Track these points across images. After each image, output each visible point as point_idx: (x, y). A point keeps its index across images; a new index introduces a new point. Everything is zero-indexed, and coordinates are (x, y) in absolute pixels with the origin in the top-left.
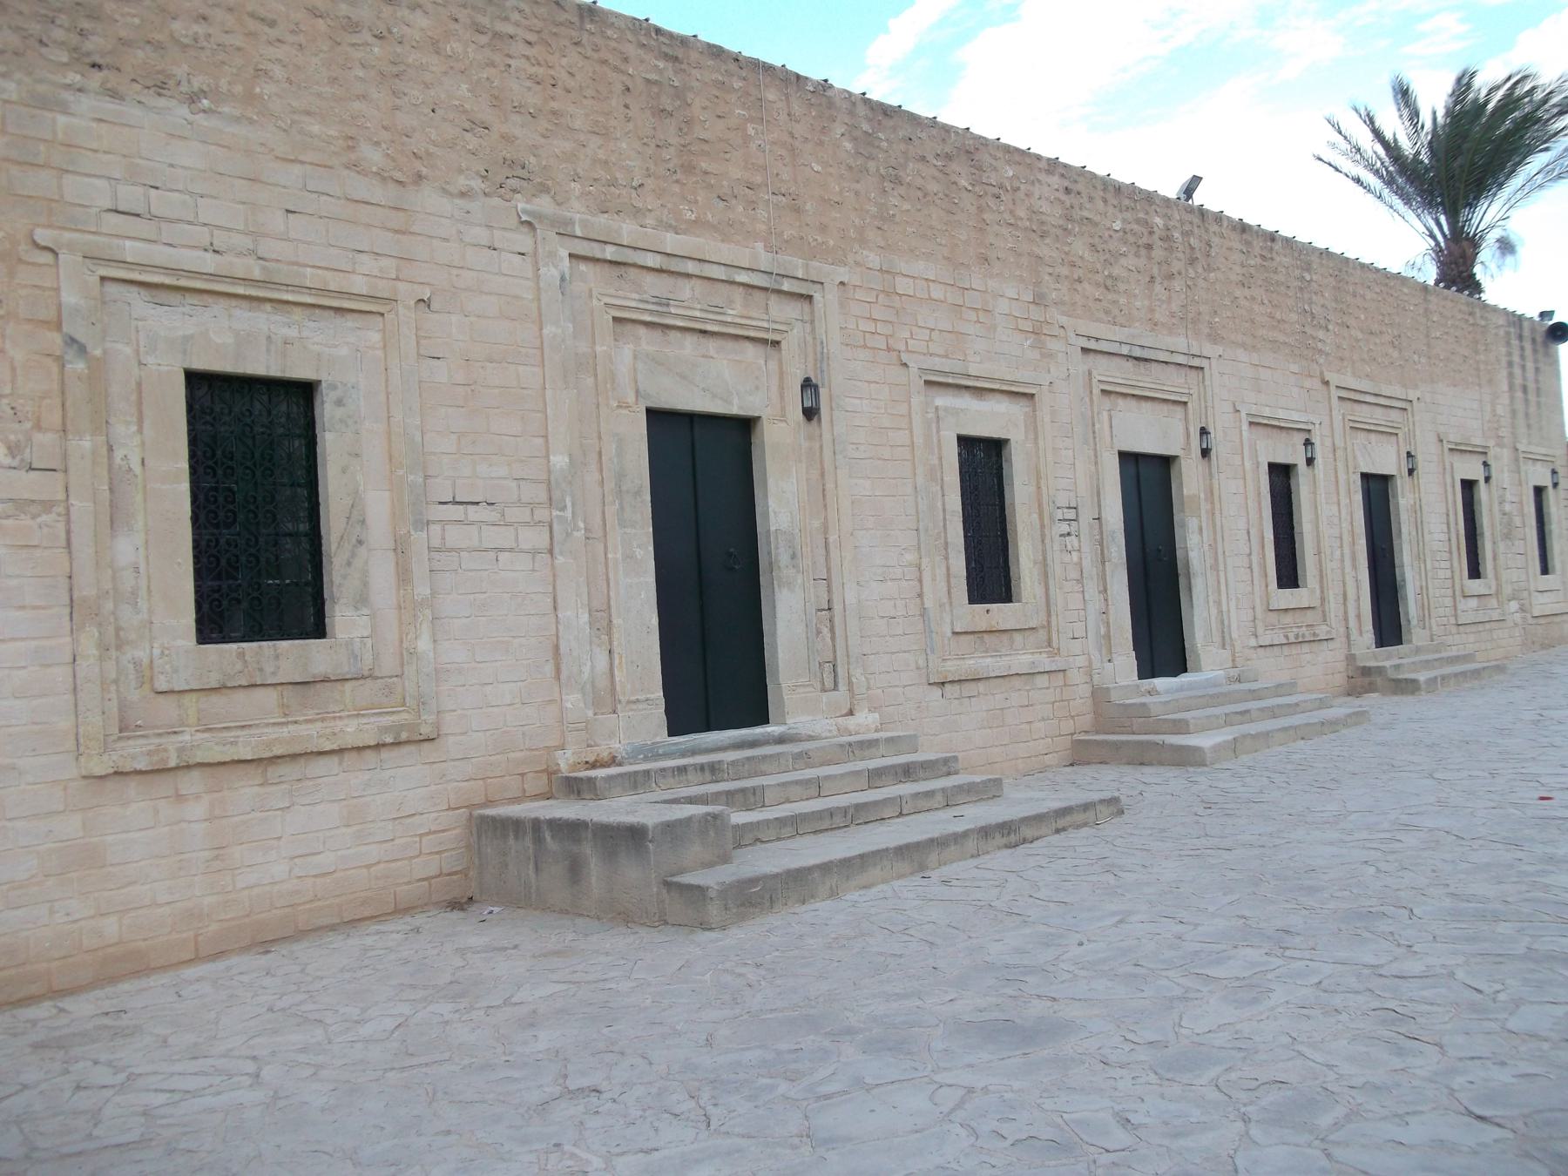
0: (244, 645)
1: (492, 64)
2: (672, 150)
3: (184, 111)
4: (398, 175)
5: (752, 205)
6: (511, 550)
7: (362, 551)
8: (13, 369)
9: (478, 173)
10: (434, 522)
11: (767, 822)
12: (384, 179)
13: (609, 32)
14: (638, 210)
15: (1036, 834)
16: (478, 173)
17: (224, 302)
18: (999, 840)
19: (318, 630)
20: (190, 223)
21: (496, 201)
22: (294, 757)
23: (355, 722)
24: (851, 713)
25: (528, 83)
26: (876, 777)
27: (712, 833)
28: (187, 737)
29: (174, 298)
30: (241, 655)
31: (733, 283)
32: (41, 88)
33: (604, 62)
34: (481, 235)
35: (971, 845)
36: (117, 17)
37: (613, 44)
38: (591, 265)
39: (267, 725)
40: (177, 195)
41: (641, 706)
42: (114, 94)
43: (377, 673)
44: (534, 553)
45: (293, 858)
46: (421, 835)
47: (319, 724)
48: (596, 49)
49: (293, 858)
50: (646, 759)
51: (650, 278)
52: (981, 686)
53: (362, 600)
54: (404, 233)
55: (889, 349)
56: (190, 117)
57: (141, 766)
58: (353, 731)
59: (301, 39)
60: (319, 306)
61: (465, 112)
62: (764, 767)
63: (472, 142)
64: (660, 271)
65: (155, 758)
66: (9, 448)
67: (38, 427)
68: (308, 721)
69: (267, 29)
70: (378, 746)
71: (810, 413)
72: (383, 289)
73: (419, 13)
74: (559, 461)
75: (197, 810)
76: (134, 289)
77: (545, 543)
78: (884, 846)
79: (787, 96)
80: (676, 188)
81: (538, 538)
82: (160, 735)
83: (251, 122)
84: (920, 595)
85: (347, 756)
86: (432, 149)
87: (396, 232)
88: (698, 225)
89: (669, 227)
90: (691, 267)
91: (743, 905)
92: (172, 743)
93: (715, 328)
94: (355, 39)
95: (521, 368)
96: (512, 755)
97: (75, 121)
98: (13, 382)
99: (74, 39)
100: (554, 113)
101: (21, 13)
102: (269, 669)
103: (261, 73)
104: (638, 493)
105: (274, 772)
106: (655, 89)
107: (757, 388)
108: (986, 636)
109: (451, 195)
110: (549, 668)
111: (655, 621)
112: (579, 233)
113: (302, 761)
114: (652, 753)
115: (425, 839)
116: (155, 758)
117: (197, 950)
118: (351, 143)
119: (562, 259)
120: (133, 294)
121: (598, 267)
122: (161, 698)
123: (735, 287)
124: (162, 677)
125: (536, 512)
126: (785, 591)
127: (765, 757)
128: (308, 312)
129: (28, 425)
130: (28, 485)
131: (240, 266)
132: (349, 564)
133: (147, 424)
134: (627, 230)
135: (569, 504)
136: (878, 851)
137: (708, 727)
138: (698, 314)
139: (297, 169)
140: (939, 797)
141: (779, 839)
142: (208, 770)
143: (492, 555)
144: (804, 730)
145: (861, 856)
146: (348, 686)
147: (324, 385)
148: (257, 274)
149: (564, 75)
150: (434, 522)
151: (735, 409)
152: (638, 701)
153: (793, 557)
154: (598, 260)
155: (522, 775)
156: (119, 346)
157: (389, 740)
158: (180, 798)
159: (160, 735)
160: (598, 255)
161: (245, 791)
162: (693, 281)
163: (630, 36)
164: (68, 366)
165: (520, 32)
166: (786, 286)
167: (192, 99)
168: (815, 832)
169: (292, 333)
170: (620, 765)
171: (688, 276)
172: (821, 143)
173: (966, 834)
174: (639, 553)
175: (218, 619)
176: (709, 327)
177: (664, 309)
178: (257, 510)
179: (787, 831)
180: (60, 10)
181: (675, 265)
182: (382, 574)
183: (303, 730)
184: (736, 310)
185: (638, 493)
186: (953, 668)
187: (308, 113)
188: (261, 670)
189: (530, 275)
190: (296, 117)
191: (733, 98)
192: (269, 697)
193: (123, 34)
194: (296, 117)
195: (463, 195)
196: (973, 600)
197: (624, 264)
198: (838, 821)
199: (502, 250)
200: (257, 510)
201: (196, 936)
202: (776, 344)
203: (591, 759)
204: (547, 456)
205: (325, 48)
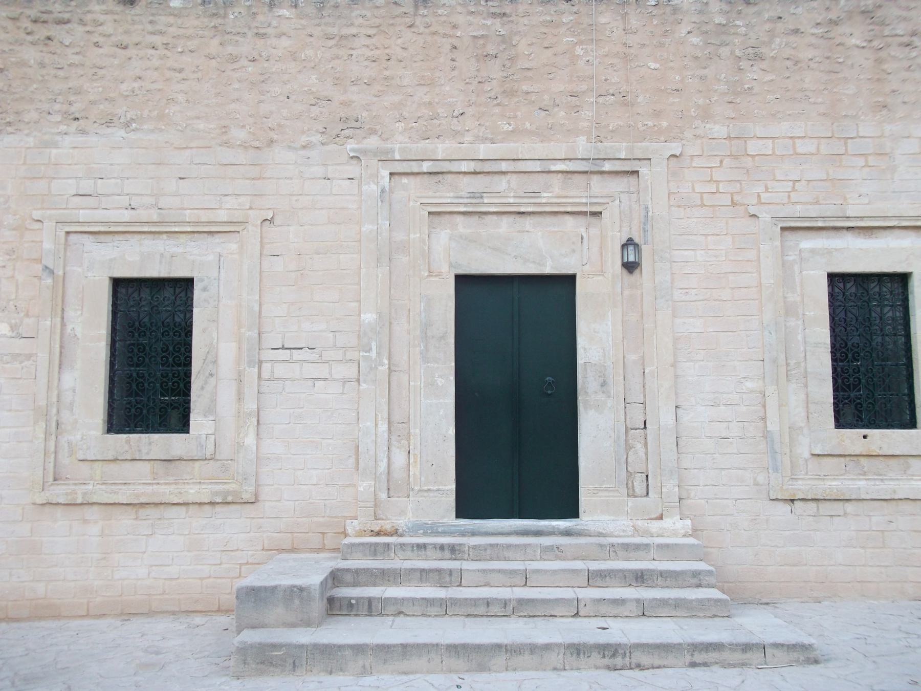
0: (131, 435)
1: (338, 57)
2: (494, 83)
3: (122, 133)
4: (257, 144)
5: (577, 109)
6: (326, 379)
7: (212, 380)
8: (17, 286)
9: (317, 131)
10: (266, 362)
11: (413, 601)
12: (245, 147)
13: (440, 12)
14: (457, 133)
15: (657, 662)
16: (317, 131)
17: (137, 237)
18: (596, 658)
19: (184, 427)
20: (119, 195)
21: (332, 147)
22: (156, 505)
23: (197, 487)
24: (661, 518)
25: (366, 63)
26: (594, 578)
27: (297, 602)
28: (90, 487)
29: (108, 238)
30: (128, 442)
31: (549, 172)
32: (46, 137)
33: (435, 33)
34: (318, 171)
35: (554, 658)
36: (90, 90)
37: (443, 19)
38: (412, 178)
39: (140, 484)
40: (113, 180)
41: (431, 494)
42: (83, 132)
43: (217, 457)
44: (344, 381)
45: (152, 566)
46: (241, 565)
47: (174, 486)
48: (428, 26)
49: (152, 566)
50: (425, 534)
51: (466, 179)
52: (850, 507)
53: (211, 410)
54: (259, 179)
55: (734, 204)
56: (125, 135)
57: (61, 501)
58: (193, 492)
59: (199, 75)
60: (198, 232)
61: (313, 93)
63: (315, 110)
64: (475, 173)
65: (69, 497)
66: (11, 327)
67: (27, 315)
68: (166, 484)
69: (177, 75)
70: (212, 503)
71: (630, 267)
72: (238, 216)
73: (284, 38)
74: (369, 317)
75: (95, 529)
76: (86, 236)
77: (355, 375)
78: (435, 641)
79: (623, 17)
80: (497, 110)
81: (351, 371)
82: (75, 484)
83: (161, 130)
84: (764, 419)
85: (191, 507)
86: (283, 122)
87: (253, 179)
88: (515, 133)
89: (484, 140)
90: (504, 166)
91: (263, 663)
92: (80, 490)
93: (530, 209)
94: (235, 66)
95: (341, 256)
96: (316, 519)
97: (60, 150)
98: (17, 292)
99: (65, 107)
100: (386, 78)
101: (40, 101)
102: (144, 451)
103: (171, 101)
105: (143, 512)
106: (481, 42)
107: (574, 251)
108: (862, 459)
109: (295, 149)
110: (352, 460)
111: (452, 431)
112: (397, 157)
113: (162, 507)
114: (433, 530)
115: (243, 568)
116: (69, 497)
117: (88, 610)
118: (225, 129)
119: (383, 177)
120: (86, 239)
121: (419, 179)
122: (81, 463)
123: (552, 175)
124: (81, 452)
125: (348, 353)
126: (592, 412)
127: (509, 546)
128: (190, 236)
129: (22, 314)
130: (19, 346)
131: (143, 214)
132: (202, 388)
134: (441, 149)
135: (374, 348)
136: (426, 645)
137: (521, 516)
138: (511, 200)
139: (187, 153)
140: (632, 608)
141: (423, 615)
142: (103, 507)
143: (310, 383)
144: (592, 527)
145: (404, 646)
146: (197, 464)
148: (155, 218)
149: (399, 50)
150: (266, 362)
151: (548, 269)
152: (429, 490)
153: (604, 384)
154: (418, 174)
155: (323, 533)
156: (75, 268)
157: (219, 500)
158: (85, 521)
159: (75, 484)
160: (416, 170)
161: (125, 521)
162: (509, 176)
163: (459, 9)
165: (364, 31)
166: (607, 167)
167: (127, 125)
168: (530, 616)
169: (180, 250)
170: (401, 536)
171: (504, 173)
172: (662, 45)
173: (547, 647)
174: (440, 382)
176: (523, 209)
177: (481, 201)
178: (151, 360)
179: (433, 610)
180: (59, 94)
181: (487, 167)
182: (226, 395)
183: (162, 489)
184: (553, 192)
185: (443, 337)
186: (802, 487)
187: (198, 118)
188: (140, 451)
189: (356, 192)
190: (189, 122)
191: (562, 30)
192: (145, 467)
193: (92, 98)
194: (189, 122)
195: (304, 147)
196: (840, 423)
197: (442, 173)
198: (494, 610)
199: (334, 179)
200: (151, 360)
201: (88, 603)
202: (597, 214)
203: (377, 529)
204: (359, 315)
205: (214, 77)
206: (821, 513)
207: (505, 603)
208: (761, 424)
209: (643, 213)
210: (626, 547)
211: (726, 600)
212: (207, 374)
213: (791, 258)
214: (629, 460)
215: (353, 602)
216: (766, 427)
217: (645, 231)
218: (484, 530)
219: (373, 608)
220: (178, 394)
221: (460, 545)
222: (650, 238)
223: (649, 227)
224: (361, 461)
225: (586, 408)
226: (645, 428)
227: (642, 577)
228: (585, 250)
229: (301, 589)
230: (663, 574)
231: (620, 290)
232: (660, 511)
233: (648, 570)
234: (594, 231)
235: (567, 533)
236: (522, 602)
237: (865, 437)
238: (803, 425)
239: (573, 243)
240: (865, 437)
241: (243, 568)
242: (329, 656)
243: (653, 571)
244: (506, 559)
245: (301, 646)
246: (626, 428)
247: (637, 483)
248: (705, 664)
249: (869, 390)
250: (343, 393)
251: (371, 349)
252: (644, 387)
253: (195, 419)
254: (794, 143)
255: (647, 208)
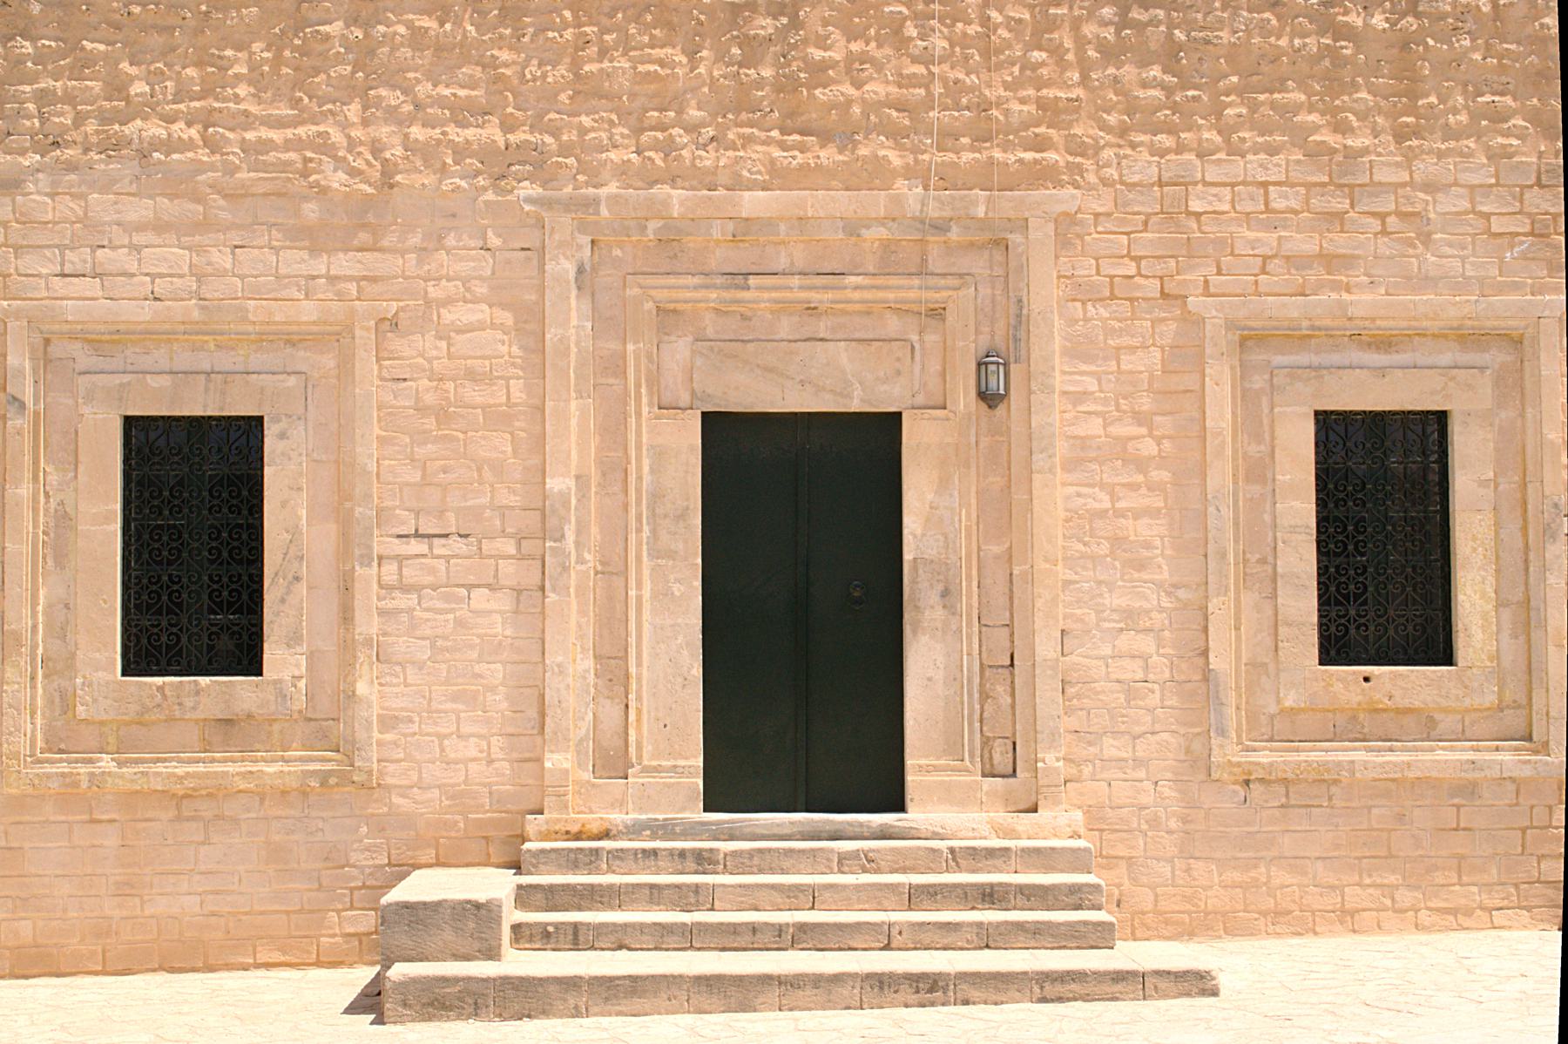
18: (906, 993)
26: (915, 897)
46: (352, 890)
62: (786, 864)
71: (989, 398)
77: (537, 580)
84: (1205, 653)
104: (682, 516)
107: (899, 373)
111: (697, 671)
114: (665, 830)
132: (283, 601)
133: (81, 469)
147: (266, 419)
164: (9, 423)
174: (677, 589)
175: (1428, 433)
179: (672, 941)
185: (682, 516)
198: (766, 938)
200: (195, 550)
206: (1293, 802)
207: (780, 929)
208: (1200, 661)
209: (1013, 309)
210: (973, 852)
211: (1112, 924)
212: (290, 577)
213: (1257, 386)
214: (986, 715)
215: (551, 929)
216: (1208, 663)
217: (1016, 340)
218: (748, 830)
219: (581, 938)
220: (239, 611)
221: (711, 850)
222: (1023, 352)
223: (1022, 334)
224: (548, 720)
225: (915, 632)
226: (1012, 665)
227: (991, 895)
228: (917, 368)
229: (478, 906)
230: (1022, 889)
231: (973, 440)
232: (1033, 799)
233: (1000, 884)
234: (931, 338)
235: (884, 834)
236: (802, 928)
237: (1366, 679)
238: (1266, 660)
239: (898, 359)
240: (1366, 679)
241: (356, 893)
242: (523, 998)
243: (1010, 885)
244: (783, 872)
245: (486, 980)
246: (981, 664)
247: (1005, 763)
248: (1060, 1000)
249: (1380, 603)
250: (1517, 804)
251: (563, 536)
252: (1011, 598)
253: (272, 653)
254: (1266, 193)
255: (1020, 301)
